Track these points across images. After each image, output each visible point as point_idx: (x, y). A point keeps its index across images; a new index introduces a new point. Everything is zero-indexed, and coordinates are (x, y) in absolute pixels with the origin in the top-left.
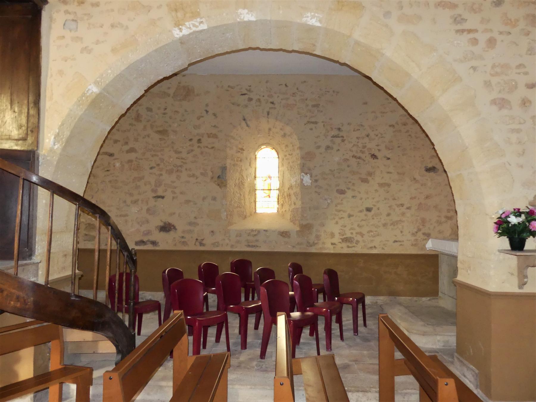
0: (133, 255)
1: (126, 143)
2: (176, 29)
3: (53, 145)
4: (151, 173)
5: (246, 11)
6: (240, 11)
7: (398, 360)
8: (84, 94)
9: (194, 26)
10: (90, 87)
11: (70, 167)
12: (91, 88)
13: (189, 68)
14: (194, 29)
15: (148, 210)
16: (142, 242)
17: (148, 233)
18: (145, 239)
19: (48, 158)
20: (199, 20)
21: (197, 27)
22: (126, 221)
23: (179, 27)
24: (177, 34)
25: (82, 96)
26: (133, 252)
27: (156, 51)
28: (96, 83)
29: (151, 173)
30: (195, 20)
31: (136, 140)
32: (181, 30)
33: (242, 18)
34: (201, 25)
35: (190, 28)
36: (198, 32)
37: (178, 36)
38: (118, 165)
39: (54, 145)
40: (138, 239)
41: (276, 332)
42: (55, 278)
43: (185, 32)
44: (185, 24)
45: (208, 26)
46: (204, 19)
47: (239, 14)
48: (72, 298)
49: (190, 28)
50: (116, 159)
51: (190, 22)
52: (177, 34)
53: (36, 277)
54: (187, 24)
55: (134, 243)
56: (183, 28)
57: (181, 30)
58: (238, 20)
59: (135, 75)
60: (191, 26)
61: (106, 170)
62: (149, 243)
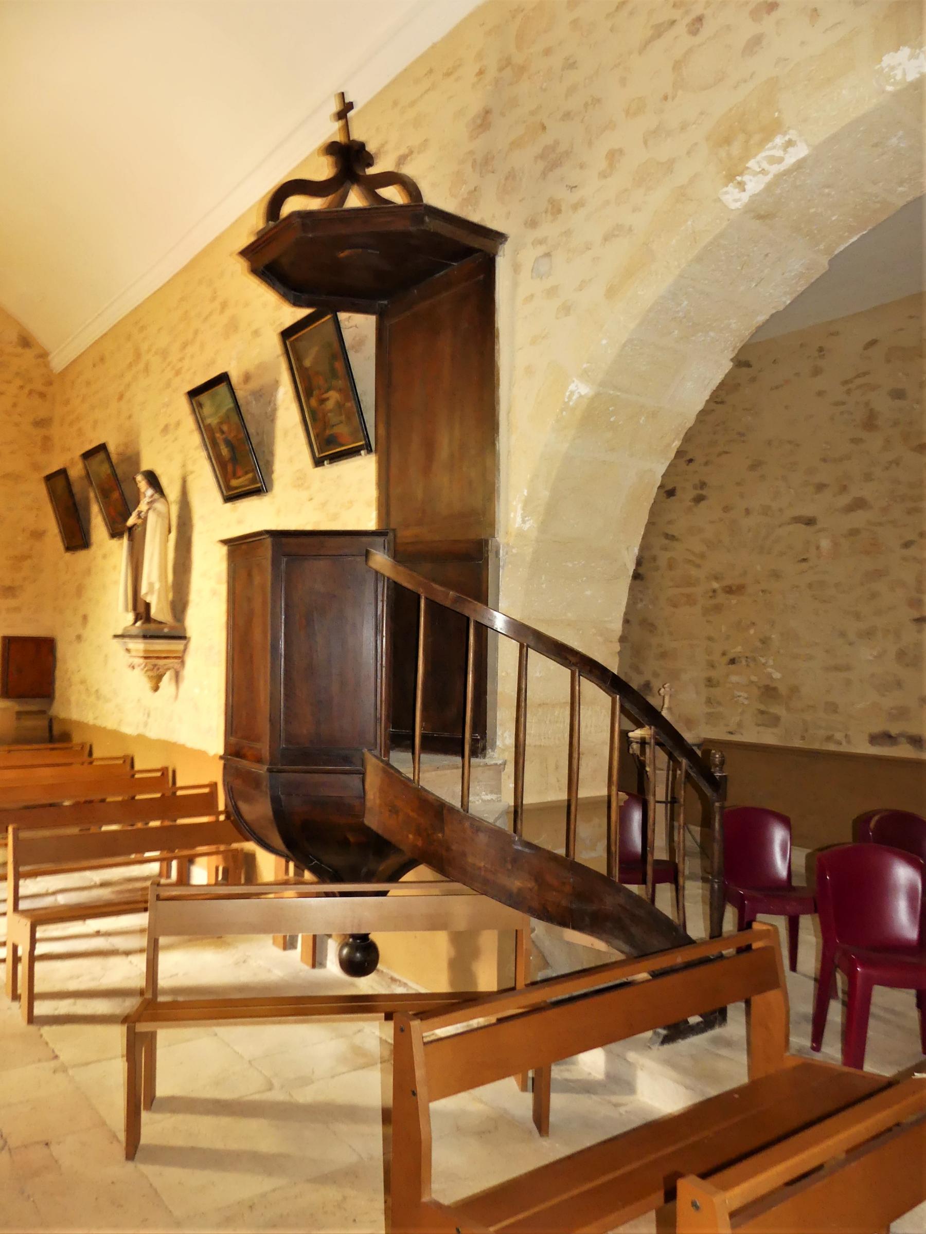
0: (716, 766)
1: (844, 489)
2: (731, 188)
3: (521, 522)
4: (904, 559)
5: (905, 51)
6: (888, 60)
9: (773, 160)
11: (570, 565)
12: (576, 388)
14: (775, 169)
15: (901, 655)
16: (886, 738)
17: (901, 713)
18: (894, 731)
20: (779, 140)
21: (780, 160)
22: (848, 683)
23: (736, 179)
24: (736, 201)
26: (717, 760)
27: (699, 259)
28: (585, 375)
29: (904, 559)
30: (770, 145)
31: (868, 477)
32: (742, 186)
34: (790, 150)
35: (763, 172)
36: (787, 173)
37: (738, 205)
38: (825, 544)
39: (524, 522)
40: (877, 729)
42: (549, 799)
43: (754, 185)
44: (748, 168)
45: (808, 145)
46: (791, 131)
47: (887, 70)
48: (516, 847)
49: (763, 172)
50: (820, 531)
51: (759, 158)
52: (736, 201)
53: (496, 794)
54: (752, 164)
55: (867, 738)
56: (746, 178)
57: (742, 186)
58: (890, 88)
59: (676, 332)
60: (765, 165)
61: (800, 559)
62: (903, 740)
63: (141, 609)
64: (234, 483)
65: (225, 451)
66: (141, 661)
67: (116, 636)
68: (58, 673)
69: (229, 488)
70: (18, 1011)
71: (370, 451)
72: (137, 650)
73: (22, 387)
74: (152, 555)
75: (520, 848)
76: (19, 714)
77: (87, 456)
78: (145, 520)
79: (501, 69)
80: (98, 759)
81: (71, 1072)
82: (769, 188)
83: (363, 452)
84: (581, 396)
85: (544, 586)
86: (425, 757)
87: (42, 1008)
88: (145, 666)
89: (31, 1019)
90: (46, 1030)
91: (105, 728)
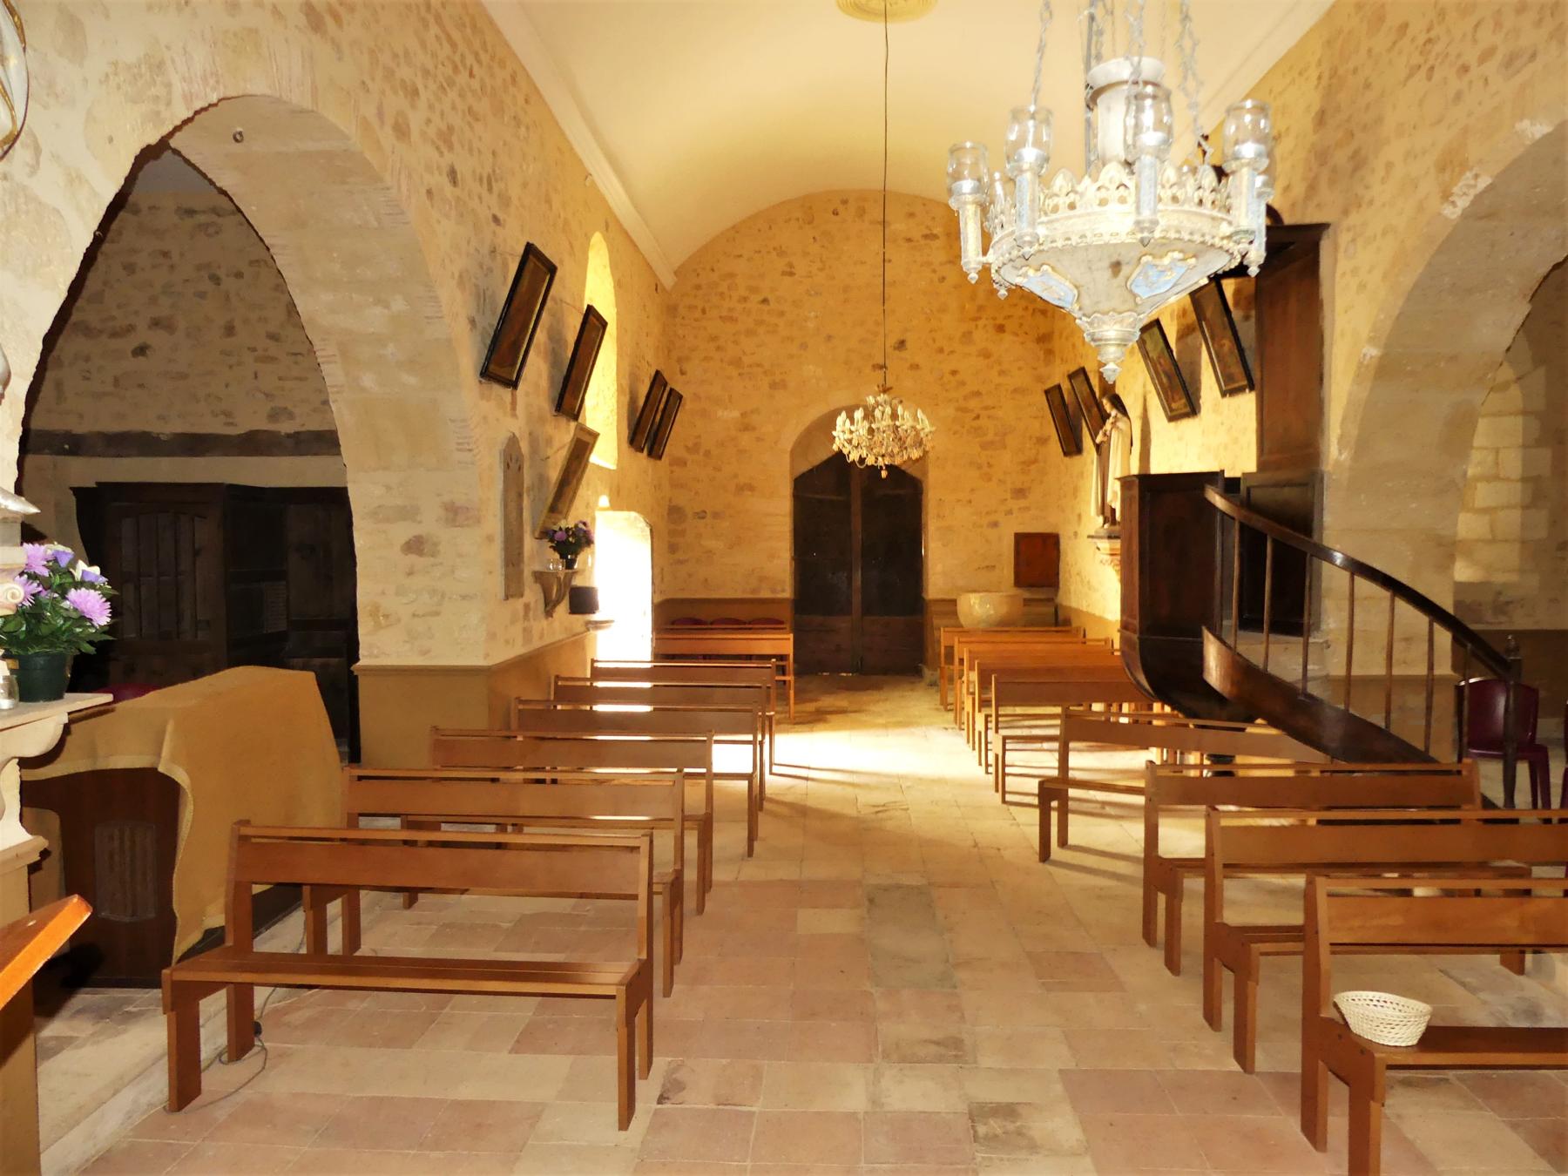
2: (1446, 205)
7: (670, 828)
8: (1360, 364)
10: (1364, 350)
13: (197, 117)
14: (1473, 193)
19: (1334, 477)
20: (1469, 175)
25: (1359, 368)
33: (1530, 136)
39: (1340, 453)
41: (644, 743)
43: (1463, 203)
52: (1453, 213)
60: (1465, 190)
63: (1108, 513)
64: (1174, 406)
65: (1165, 380)
66: (1108, 557)
67: (1089, 537)
68: (1062, 565)
69: (1171, 410)
70: (998, 796)
71: (1252, 388)
72: (1105, 549)
73: (1027, 308)
74: (1115, 468)
75: (1303, 699)
76: (1027, 602)
77: (1071, 377)
78: (1109, 438)
79: (1331, 78)
80: (1090, 640)
81: (1021, 827)
82: (1473, 203)
83: (1247, 390)
84: (1371, 357)
85: (1364, 503)
86: (1273, 637)
87: (1009, 798)
88: (1112, 562)
89: (1004, 801)
90: (1012, 808)
91: (1094, 615)
